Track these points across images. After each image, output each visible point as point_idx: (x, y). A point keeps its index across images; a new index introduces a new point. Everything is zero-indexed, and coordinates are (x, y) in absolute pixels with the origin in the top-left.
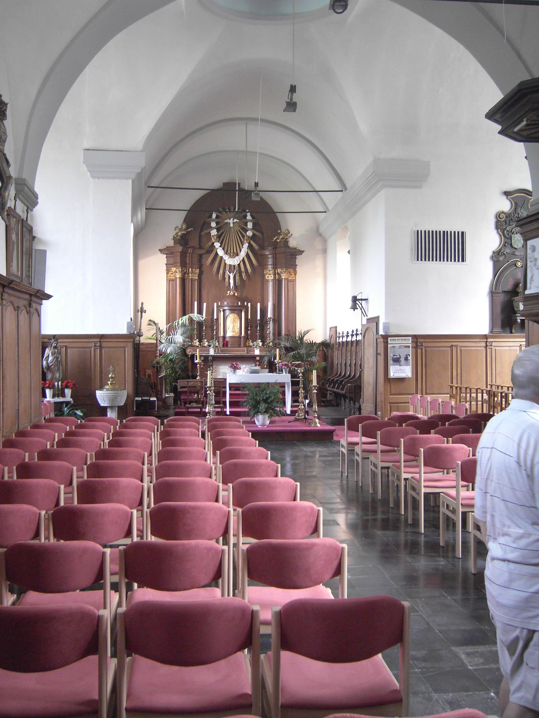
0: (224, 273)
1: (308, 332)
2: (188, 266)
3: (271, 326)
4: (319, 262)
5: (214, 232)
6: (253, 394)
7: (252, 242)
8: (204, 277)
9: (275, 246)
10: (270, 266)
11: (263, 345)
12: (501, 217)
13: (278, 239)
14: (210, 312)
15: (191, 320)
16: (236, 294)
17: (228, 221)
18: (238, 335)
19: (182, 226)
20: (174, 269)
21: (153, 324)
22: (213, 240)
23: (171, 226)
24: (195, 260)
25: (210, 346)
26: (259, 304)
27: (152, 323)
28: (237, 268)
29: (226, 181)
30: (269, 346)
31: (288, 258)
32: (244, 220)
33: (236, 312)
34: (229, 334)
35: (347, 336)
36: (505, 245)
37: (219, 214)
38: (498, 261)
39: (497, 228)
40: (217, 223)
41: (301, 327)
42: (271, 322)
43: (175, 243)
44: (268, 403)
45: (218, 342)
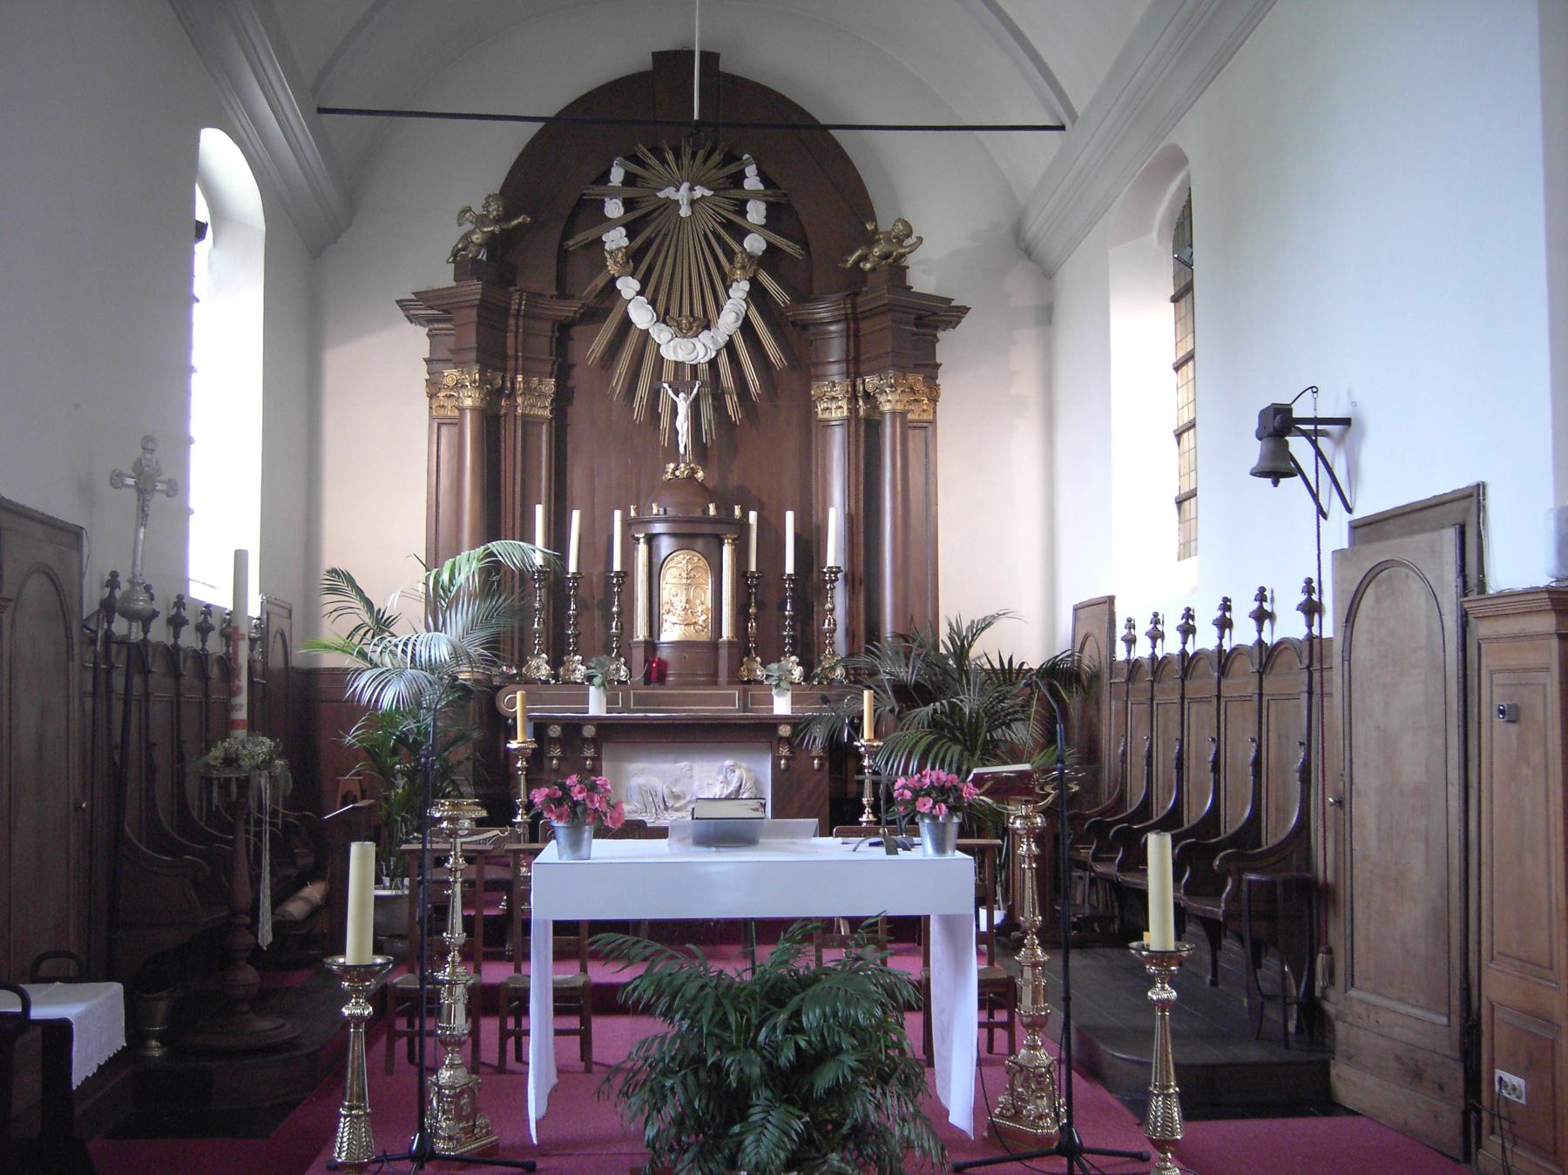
0: (655, 394)
1: (986, 623)
2: (511, 364)
3: (838, 600)
5: (616, 239)
7: (765, 279)
8: (579, 411)
9: (854, 283)
10: (835, 368)
11: (807, 677)
13: (863, 258)
14: (596, 544)
16: (700, 475)
17: (669, 192)
18: (705, 636)
19: (485, 207)
20: (451, 375)
21: (349, 590)
22: (613, 269)
23: (452, 189)
24: (543, 344)
26: (790, 516)
27: (344, 585)
29: (665, 45)
31: (909, 332)
33: (700, 543)
34: (671, 633)
40: (629, 204)
42: (839, 585)
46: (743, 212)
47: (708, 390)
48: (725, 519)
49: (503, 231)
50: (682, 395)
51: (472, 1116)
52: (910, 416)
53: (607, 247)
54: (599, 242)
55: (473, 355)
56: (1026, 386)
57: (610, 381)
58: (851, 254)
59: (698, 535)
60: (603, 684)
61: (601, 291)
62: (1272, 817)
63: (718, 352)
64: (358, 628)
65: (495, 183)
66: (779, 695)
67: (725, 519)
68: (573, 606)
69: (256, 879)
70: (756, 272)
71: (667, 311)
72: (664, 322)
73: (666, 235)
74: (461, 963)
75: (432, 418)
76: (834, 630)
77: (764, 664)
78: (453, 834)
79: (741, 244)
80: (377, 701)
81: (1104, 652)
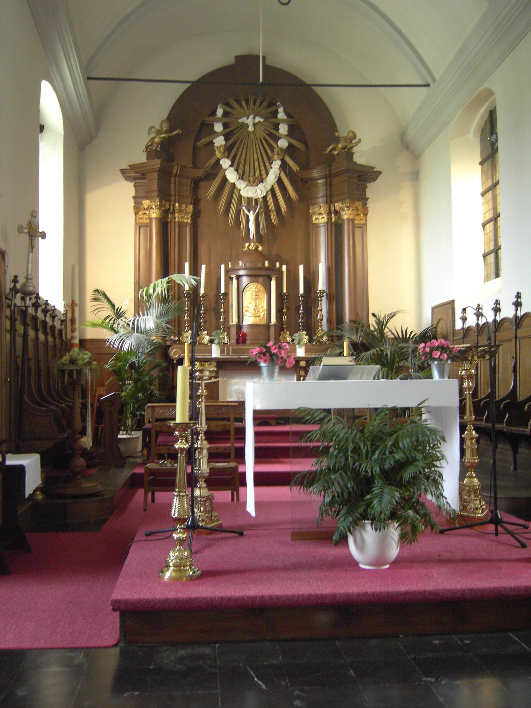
0: (238, 212)
1: (392, 316)
2: (173, 198)
3: (324, 305)
4: (405, 195)
5: (219, 141)
6: (343, 450)
7: (287, 159)
8: (203, 221)
9: (329, 160)
10: (321, 200)
11: (311, 340)
13: (334, 149)
14: (213, 281)
15: (172, 286)
16: (260, 248)
17: (244, 120)
18: (264, 322)
19: (161, 126)
20: (146, 203)
21: (103, 299)
22: (218, 155)
23: (141, 122)
24: (187, 190)
25: (212, 341)
26: (301, 267)
27: (101, 297)
28: (260, 201)
29: (241, 52)
30: (321, 343)
31: (354, 182)
32: (274, 120)
33: (261, 279)
34: (248, 320)
37: (229, 109)
40: (225, 126)
41: (378, 304)
42: (324, 299)
43: (148, 158)
44: (400, 485)
45: (229, 335)
46: (277, 129)
47: (262, 210)
48: (272, 268)
49: (169, 137)
50: (251, 212)
51: (210, 512)
52: (356, 222)
53: (215, 145)
54: (212, 143)
55: (156, 194)
56: (407, 208)
57: (218, 205)
58: (328, 147)
60: (219, 343)
61: (213, 166)
63: (267, 193)
64: (108, 317)
65: (164, 115)
66: (299, 347)
67: (272, 268)
68: (203, 309)
69: (84, 420)
70: (284, 156)
71: (243, 175)
72: (242, 179)
73: (242, 140)
74: (205, 439)
75: (136, 224)
76: (322, 320)
77: (291, 335)
78: (201, 378)
79: (277, 143)
80: (121, 347)
81: (450, 325)
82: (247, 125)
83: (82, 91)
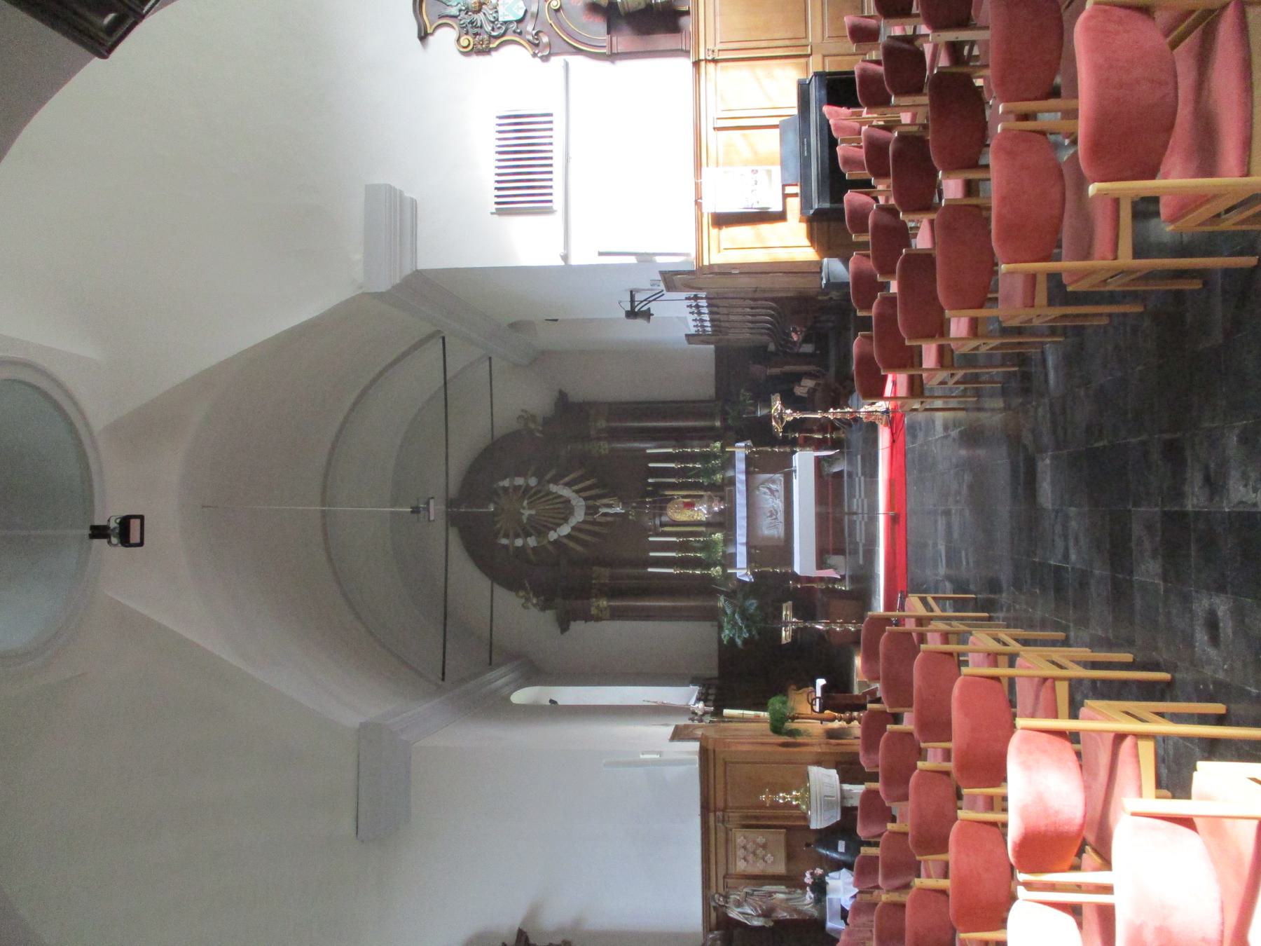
0: (600, 524)
5: (532, 542)
7: (548, 477)
12: (466, 44)
28: (590, 502)
35: (702, 321)
36: (520, 33)
38: (549, 45)
39: (487, 51)
40: (517, 536)
54: (534, 549)
59: (662, 504)
62: (720, 787)
82: (530, 516)
83: (502, 670)
